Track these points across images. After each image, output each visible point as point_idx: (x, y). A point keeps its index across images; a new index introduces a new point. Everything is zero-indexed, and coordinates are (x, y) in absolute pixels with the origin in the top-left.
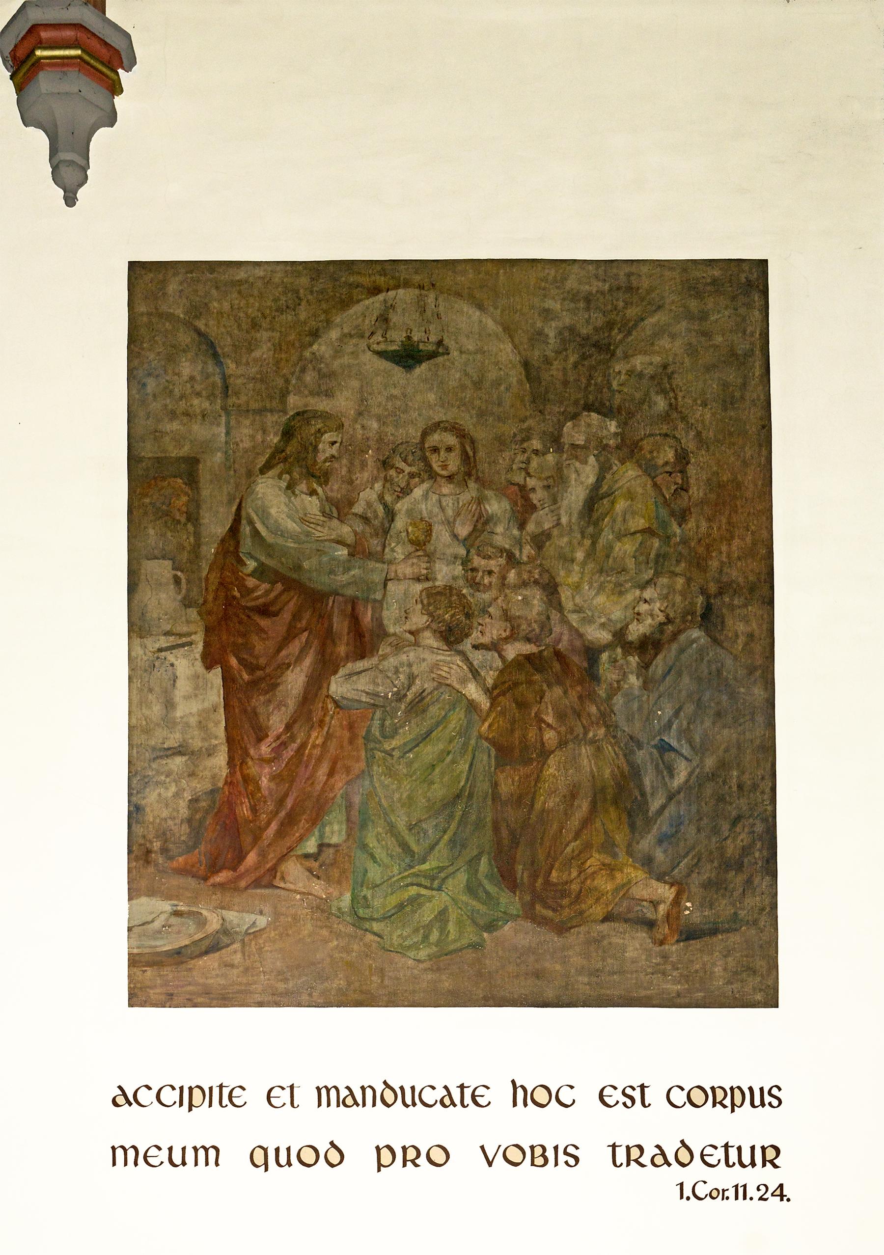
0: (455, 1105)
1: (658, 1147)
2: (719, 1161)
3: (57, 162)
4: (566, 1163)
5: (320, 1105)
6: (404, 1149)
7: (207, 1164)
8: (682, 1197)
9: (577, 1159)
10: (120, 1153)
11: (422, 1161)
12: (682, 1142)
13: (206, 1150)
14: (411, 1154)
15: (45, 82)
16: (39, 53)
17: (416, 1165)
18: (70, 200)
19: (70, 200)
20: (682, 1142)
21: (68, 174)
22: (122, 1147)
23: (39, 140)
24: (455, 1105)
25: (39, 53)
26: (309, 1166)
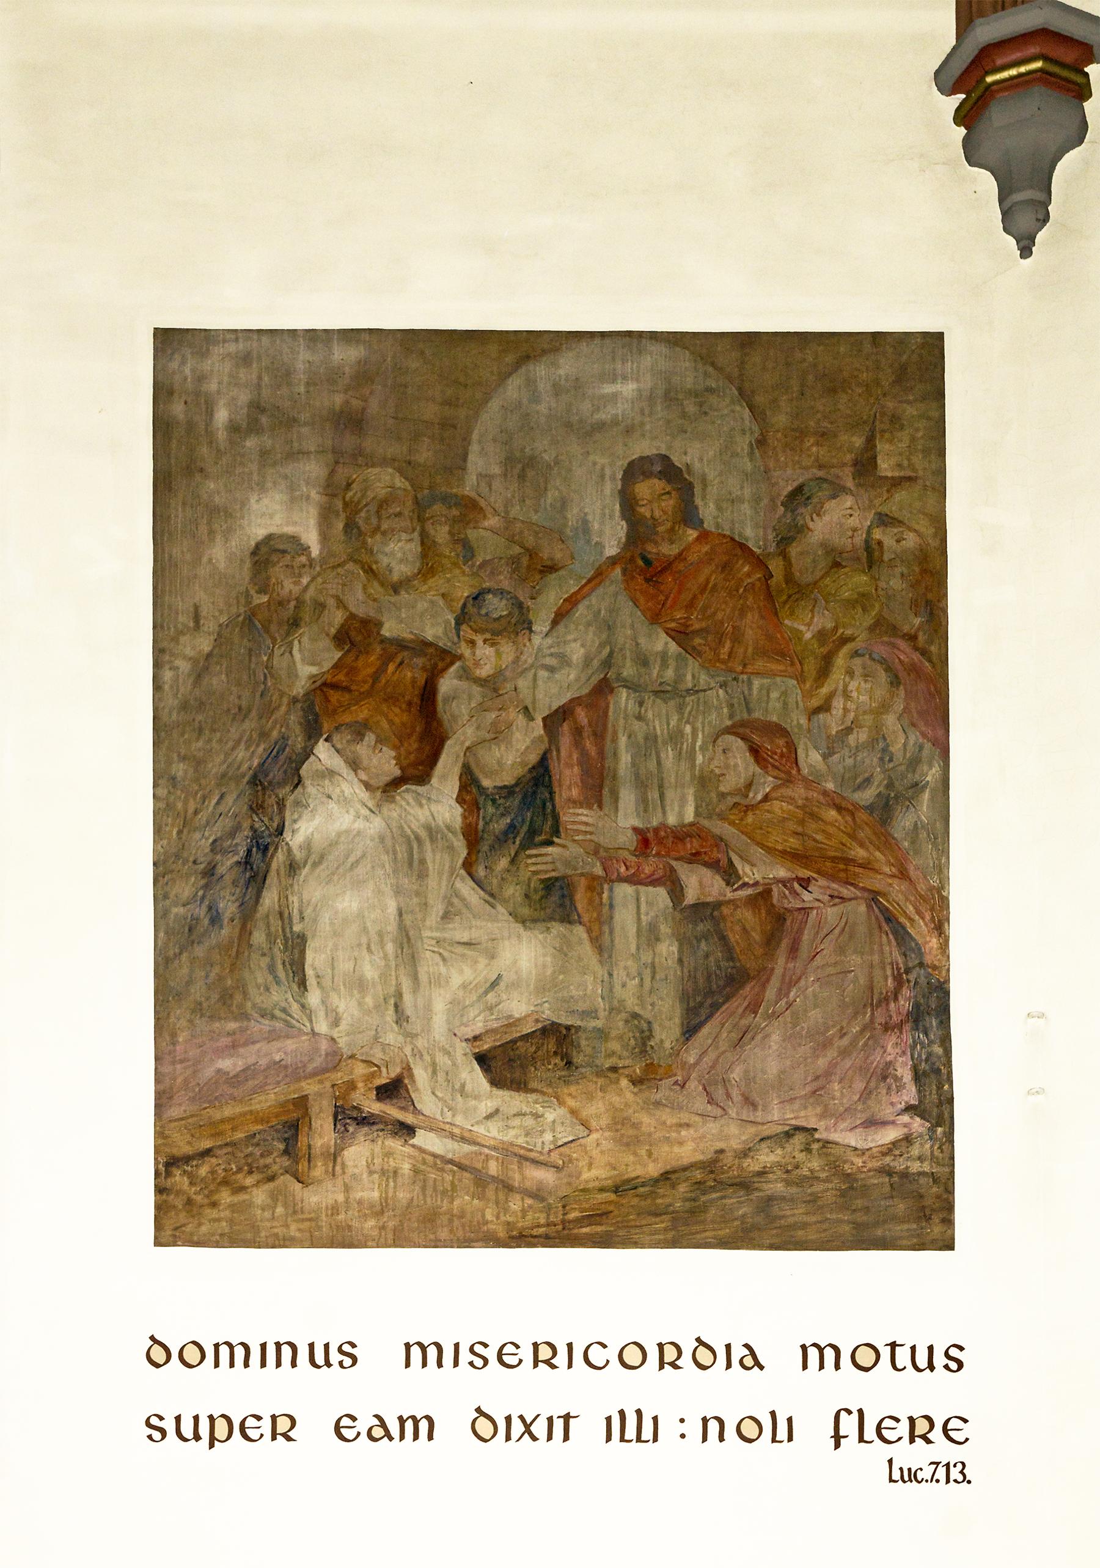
0: (391, 1439)
1: (747, 1346)
2: (359, 1434)
3: (1010, 205)
4: (471, 1364)
5: (609, 1438)
6: (661, 1346)
7: (232, 1365)
8: (861, 1412)
9: (960, 1365)
10: (416, 1352)
11: (686, 1361)
12: (152, 1338)
13: (423, 1348)
14: (670, 1354)
15: (998, 115)
16: (989, 79)
17: (553, 1367)
18: (1026, 251)
19: (1026, 251)
20: (152, 1338)
21: (1024, 220)
22: (419, 1344)
23: (986, 182)
24: (391, 1439)
25: (989, 79)
26: (867, 1370)
